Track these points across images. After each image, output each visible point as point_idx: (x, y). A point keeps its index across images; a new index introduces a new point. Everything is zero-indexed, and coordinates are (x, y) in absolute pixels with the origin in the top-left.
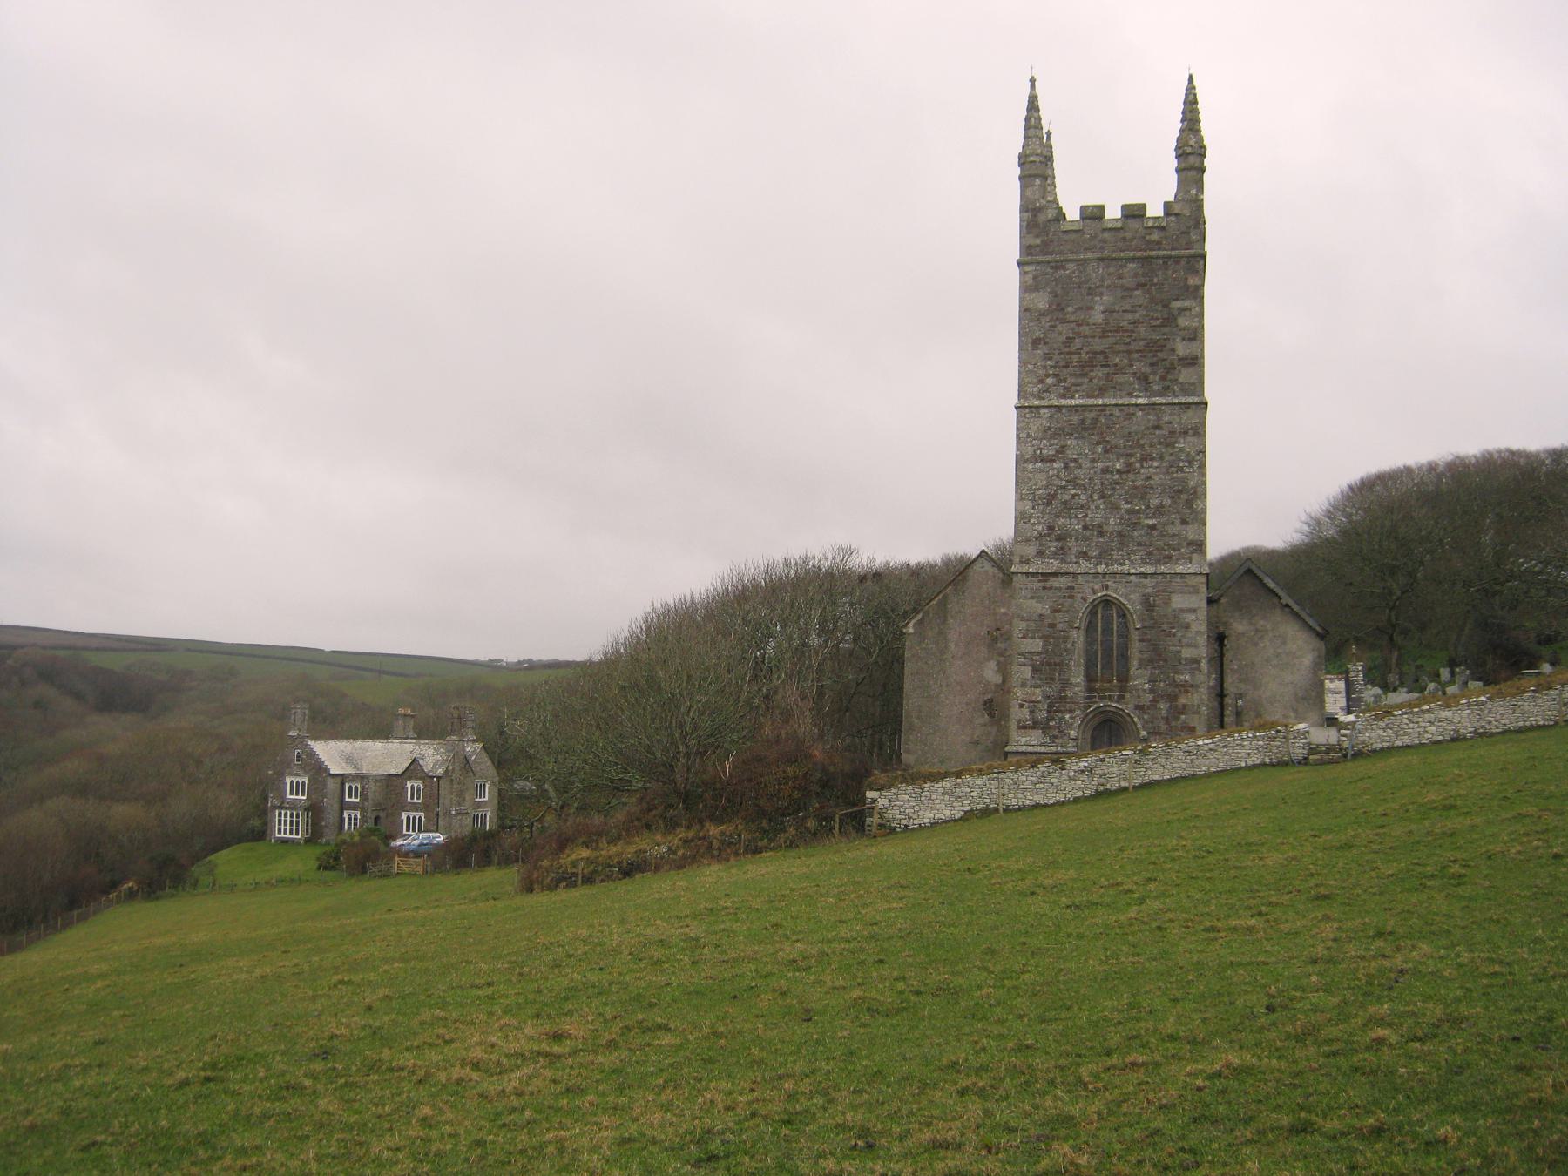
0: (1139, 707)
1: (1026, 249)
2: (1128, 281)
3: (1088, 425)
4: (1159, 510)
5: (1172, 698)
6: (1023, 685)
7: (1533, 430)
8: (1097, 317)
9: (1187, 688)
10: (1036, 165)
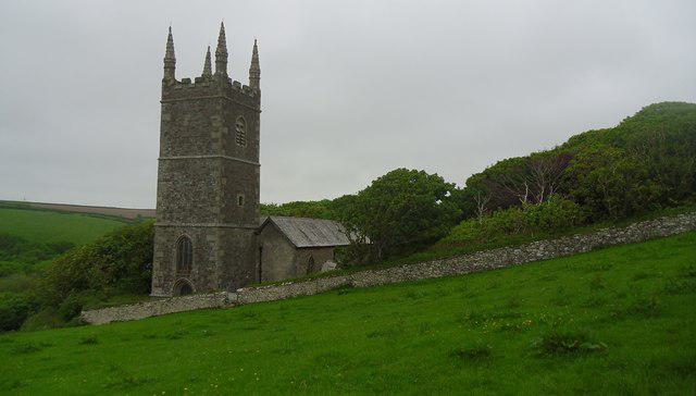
1: (164, 97)
2: (197, 109)
3: (182, 166)
4: (203, 201)
7: (682, 110)
8: (186, 123)
10: (170, 64)
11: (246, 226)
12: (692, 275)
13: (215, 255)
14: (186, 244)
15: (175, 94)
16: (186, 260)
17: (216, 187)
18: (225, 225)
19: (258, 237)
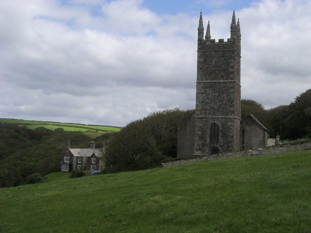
4: (225, 104)
5: (227, 144)
6: (197, 141)
8: (213, 63)
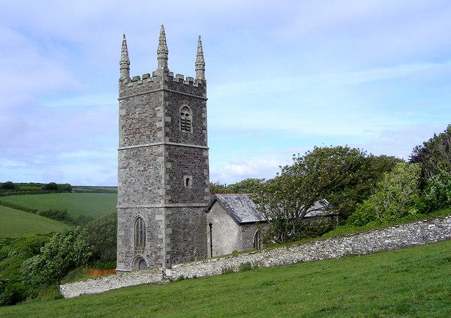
0: (148, 256)
4: (152, 184)
9: (160, 249)
10: (126, 66)
11: (195, 205)
12: (431, 209)
13: (162, 233)
14: (141, 225)
15: (131, 90)
16: (141, 237)
17: (162, 172)
18: (172, 205)
19: (208, 215)
